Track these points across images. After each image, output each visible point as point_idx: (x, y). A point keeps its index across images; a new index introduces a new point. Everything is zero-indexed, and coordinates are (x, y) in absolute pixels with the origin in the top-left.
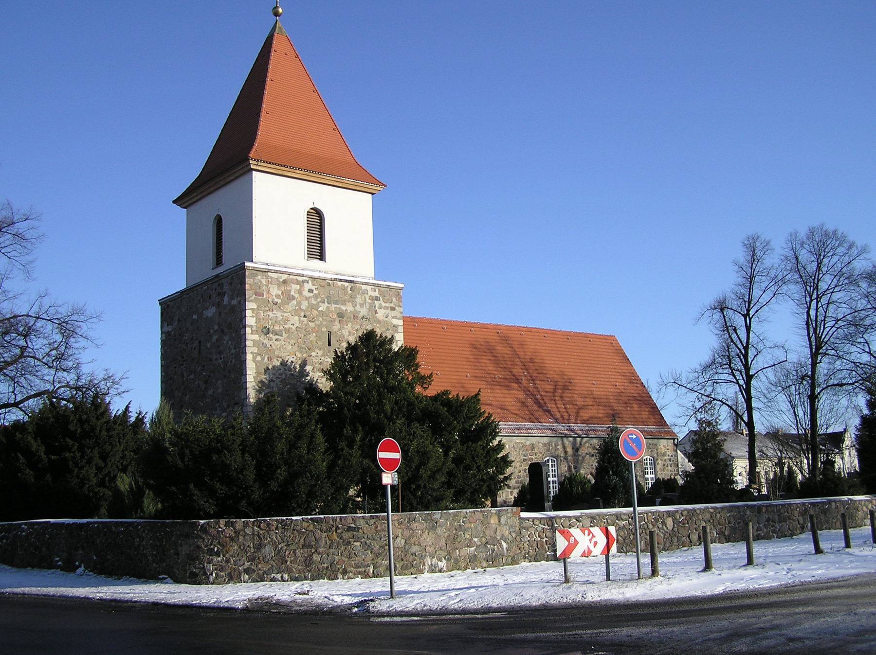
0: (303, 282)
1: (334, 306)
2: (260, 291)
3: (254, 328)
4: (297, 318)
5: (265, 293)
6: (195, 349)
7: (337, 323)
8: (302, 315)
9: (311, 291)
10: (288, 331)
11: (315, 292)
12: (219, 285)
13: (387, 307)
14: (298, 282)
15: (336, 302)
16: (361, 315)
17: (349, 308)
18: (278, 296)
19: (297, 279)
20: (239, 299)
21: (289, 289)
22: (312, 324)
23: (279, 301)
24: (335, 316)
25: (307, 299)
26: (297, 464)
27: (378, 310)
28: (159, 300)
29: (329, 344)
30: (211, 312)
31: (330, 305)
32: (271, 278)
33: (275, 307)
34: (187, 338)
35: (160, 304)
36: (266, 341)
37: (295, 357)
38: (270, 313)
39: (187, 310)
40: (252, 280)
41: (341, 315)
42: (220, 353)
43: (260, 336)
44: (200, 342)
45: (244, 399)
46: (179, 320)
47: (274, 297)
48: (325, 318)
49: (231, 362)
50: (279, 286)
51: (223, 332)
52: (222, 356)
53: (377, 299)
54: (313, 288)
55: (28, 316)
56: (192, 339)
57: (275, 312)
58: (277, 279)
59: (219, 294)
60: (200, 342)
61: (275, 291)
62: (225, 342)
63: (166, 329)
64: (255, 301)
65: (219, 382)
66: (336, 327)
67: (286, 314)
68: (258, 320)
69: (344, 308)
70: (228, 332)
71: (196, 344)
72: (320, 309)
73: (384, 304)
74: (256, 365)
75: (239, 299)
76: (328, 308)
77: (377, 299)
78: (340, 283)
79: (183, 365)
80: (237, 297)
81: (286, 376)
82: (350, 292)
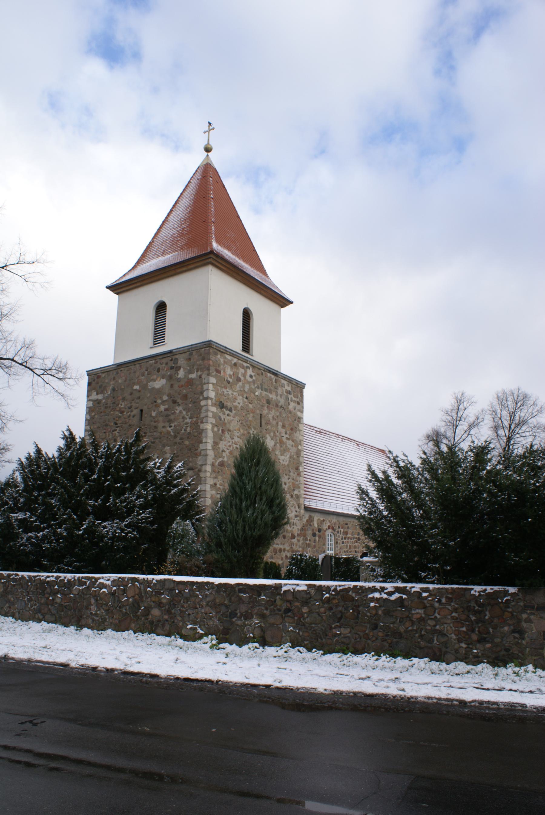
0: (247, 367)
1: (265, 393)
2: (219, 369)
3: (214, 401)
4: (241, 397)
5: (222, 372)
6: (133, 417)
7: (266, 408)
8: (245, 396)
9: (251, 376)
10: (236, 407)
11: (254, 378)
12: (172, 360)
13: (295, 401)
14: (243, 367)
15: (266, 390)
16: (280, 404)
17: (272, 396)
18: (230, 376)
19: (243, 365)
20: (199, 373)
21: (238, 371)
22: (251, 406)
23: (231, 380)
24: (265, 402)
25: (249, 383)
26: (39, 495)
27: (290, 403)
28: (87, 371)
29: (261, 426)
30: (159, 383)
31: (262, 392)
32: (227, 359)
33: (228, 385)
34: (122, 406)
35: (88, 375)
36: (221, 414)
37: (239, 433)
38: (224, 390)
39: (125, 381)
40: (214, 357)
41: (268, 402)
42: (170, 421)
43: (217, 410)
44: (142, 411)
45: (201, 465)
46: (114, 390)
47: (228, 376)
48: (259, 402)
49: (185, 430)
50: (232, 368)
51: (174, 402)
52: (173, 425)
53: (290, 393)
54: (253, 374)
55: (12, 360)
56: (130, 407)
57: (228, 390)
58: (231, 361)
59: (172, 368)
60: (142, 411)
61: (229, 371)
62: (177, 412)
63: (94, 396)
64: (215, 376)
65: (167, 448)
66: (265, 412)
67: (235, 393)
68: (217, 394)
69: (271, 396)
70: (182, 403)
71: (136, 412)
72: (256, 394)
73: (294, 399)
74: (214, 435)
75: (199, 373)
76: (261, 394)
77: (290, 393)
78: (269, 375)
79: (115, 430)
80: (197, 371)
81: (233, 448)
82: (274, 383)
